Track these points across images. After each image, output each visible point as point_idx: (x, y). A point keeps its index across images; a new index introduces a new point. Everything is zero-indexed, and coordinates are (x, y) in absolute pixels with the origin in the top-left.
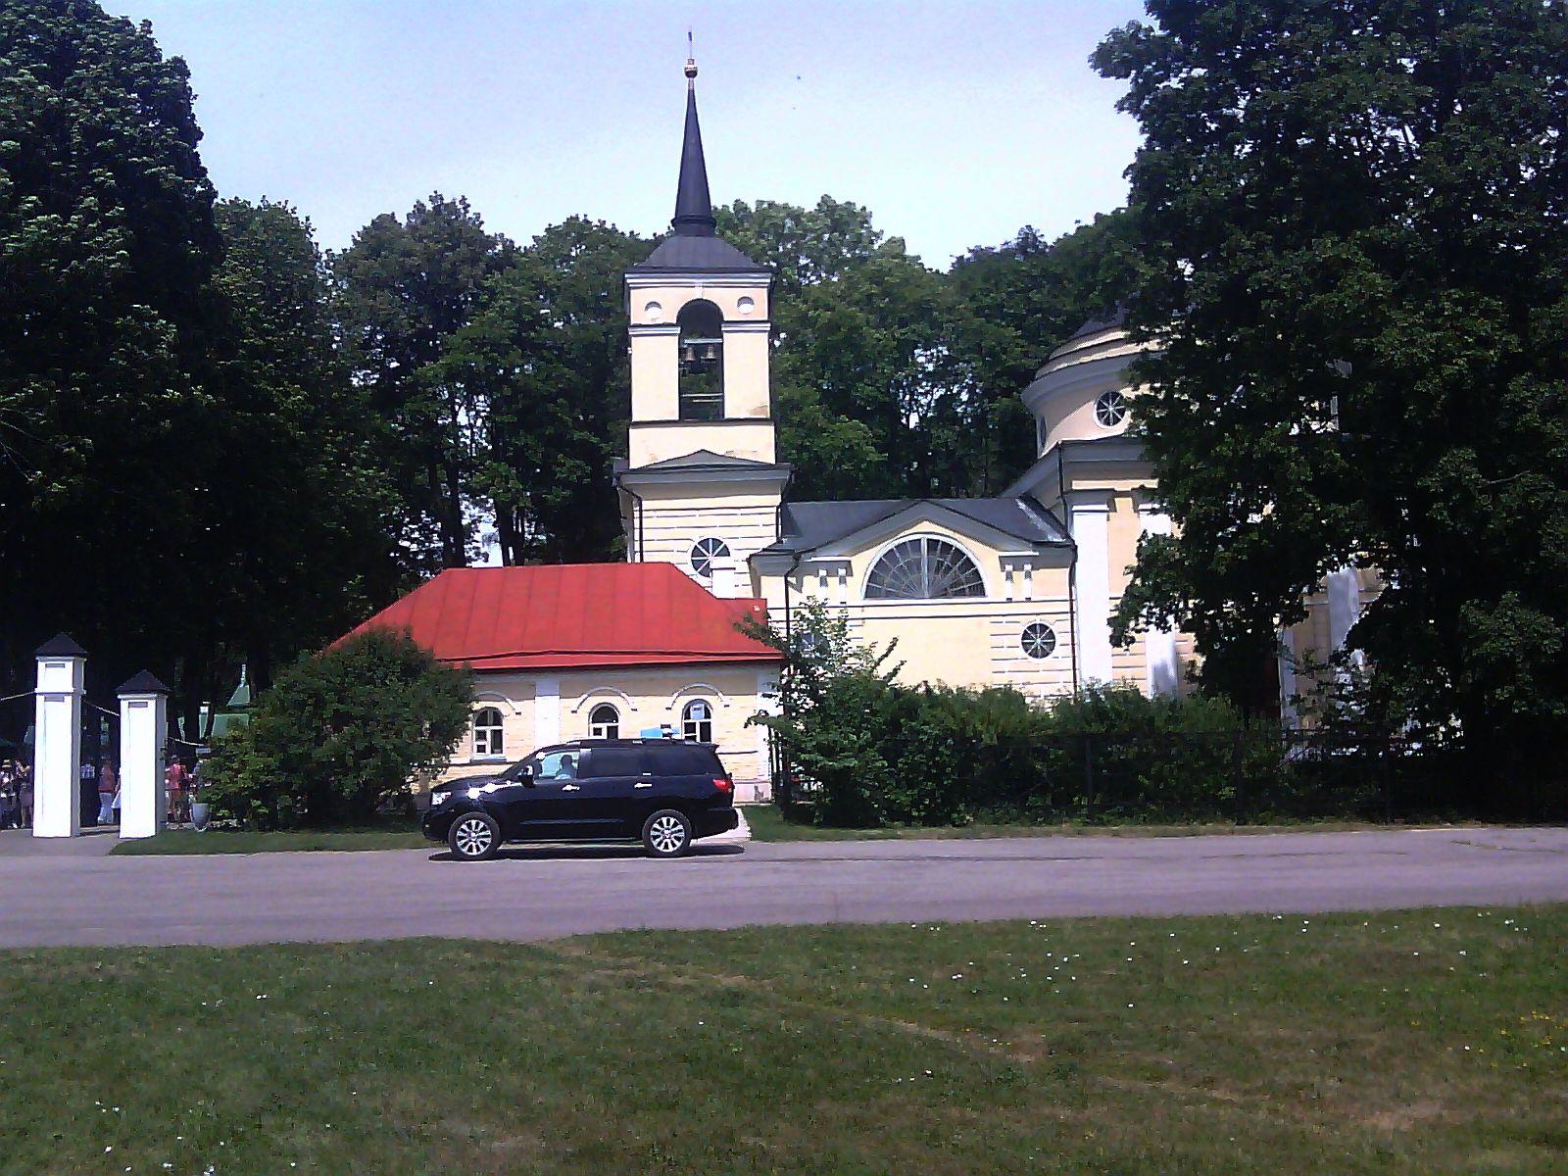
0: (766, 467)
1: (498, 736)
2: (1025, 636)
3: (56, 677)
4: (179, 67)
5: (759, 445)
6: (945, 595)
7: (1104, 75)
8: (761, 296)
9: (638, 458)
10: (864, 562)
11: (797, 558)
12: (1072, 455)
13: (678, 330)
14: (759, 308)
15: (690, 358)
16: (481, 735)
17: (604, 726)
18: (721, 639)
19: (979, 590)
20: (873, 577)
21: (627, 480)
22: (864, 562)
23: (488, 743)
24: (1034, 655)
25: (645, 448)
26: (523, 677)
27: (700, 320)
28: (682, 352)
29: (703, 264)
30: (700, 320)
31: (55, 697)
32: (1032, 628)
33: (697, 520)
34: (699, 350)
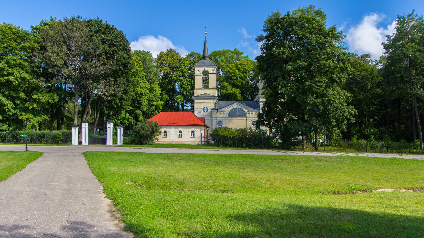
3: (110, 125)
5: (214, 93)
15: (204, 79)
16: (164, 134)
17: (180, 134)
19: (245, 115)
23: (193, 135)
25: (197, 93)
27: (206, 73)
28: (203, 77)
30: (206, 73)
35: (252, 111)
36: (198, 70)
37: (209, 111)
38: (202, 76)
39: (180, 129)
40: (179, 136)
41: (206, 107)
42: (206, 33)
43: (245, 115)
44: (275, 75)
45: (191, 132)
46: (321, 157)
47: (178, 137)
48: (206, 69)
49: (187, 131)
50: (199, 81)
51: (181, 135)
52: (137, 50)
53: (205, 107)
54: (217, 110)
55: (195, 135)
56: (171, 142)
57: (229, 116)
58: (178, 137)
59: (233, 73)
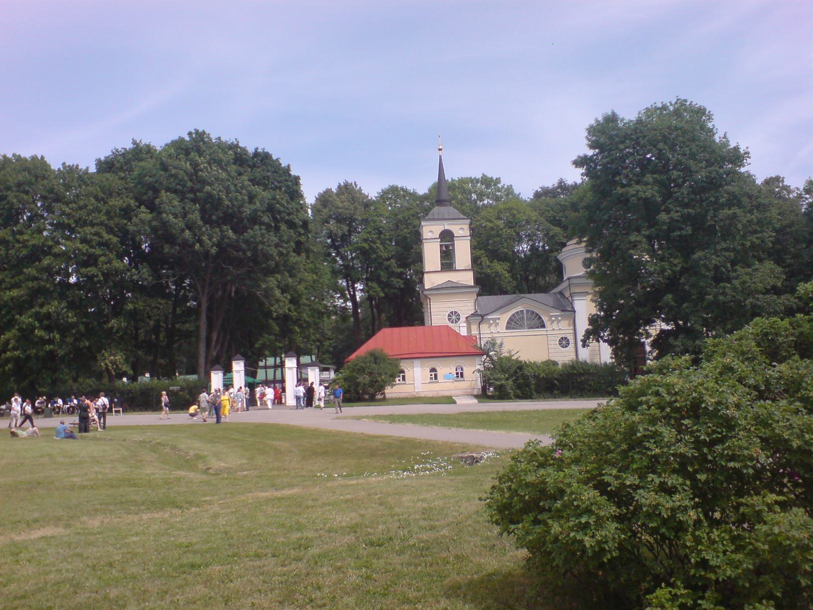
0: (471, 287)
1: (436, 375)
2: (560, 341)
4: (297, 179)
5: (468, 278)
6: (533, 328)
7: (576, 167)
8: (466, 227)
9: (427, 285)
10: (505, 318)
11: (483, 317)
12: (573, 281)
13: (439, 240)
14: (467, 233)
15: (444, 249)
17: (433, 373)
18: (464, 349)
19: (543, 326)
20: (508, 323)
21: (425, 293)
22: (505, 318)
24: (563, 347)
25: (430, 281)
26: (410, 360)
27: (447, 236)
28: (441, 246)
29: (447, 217)
30: (447, 236)
31: (238, 372)
32: (562, 338)
33: (449, 304)
34: (447, 247)
35: (556, 316)
36: (430, 231)
37: (463, 319)
38: (439, 244)
39: (433, 363)
40: (431, 378)
41: (456, 312)
42: (441, 147)
43: (543, 326)
44: (732, 228)
45: (431, 371)
46: (515, 413)
47: (429, 381)
48: (447, 227)
49: (446, 369)
50: (431, 254)
51: (436, 378)
52: (48, 160)
53: (452, 313)
54: (480, 318)
55: (465, 375)
56: (412, 394)
57: (507, 328)
58: (429, 381)
59: (492, 229)
